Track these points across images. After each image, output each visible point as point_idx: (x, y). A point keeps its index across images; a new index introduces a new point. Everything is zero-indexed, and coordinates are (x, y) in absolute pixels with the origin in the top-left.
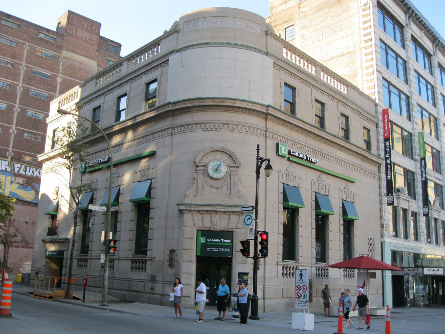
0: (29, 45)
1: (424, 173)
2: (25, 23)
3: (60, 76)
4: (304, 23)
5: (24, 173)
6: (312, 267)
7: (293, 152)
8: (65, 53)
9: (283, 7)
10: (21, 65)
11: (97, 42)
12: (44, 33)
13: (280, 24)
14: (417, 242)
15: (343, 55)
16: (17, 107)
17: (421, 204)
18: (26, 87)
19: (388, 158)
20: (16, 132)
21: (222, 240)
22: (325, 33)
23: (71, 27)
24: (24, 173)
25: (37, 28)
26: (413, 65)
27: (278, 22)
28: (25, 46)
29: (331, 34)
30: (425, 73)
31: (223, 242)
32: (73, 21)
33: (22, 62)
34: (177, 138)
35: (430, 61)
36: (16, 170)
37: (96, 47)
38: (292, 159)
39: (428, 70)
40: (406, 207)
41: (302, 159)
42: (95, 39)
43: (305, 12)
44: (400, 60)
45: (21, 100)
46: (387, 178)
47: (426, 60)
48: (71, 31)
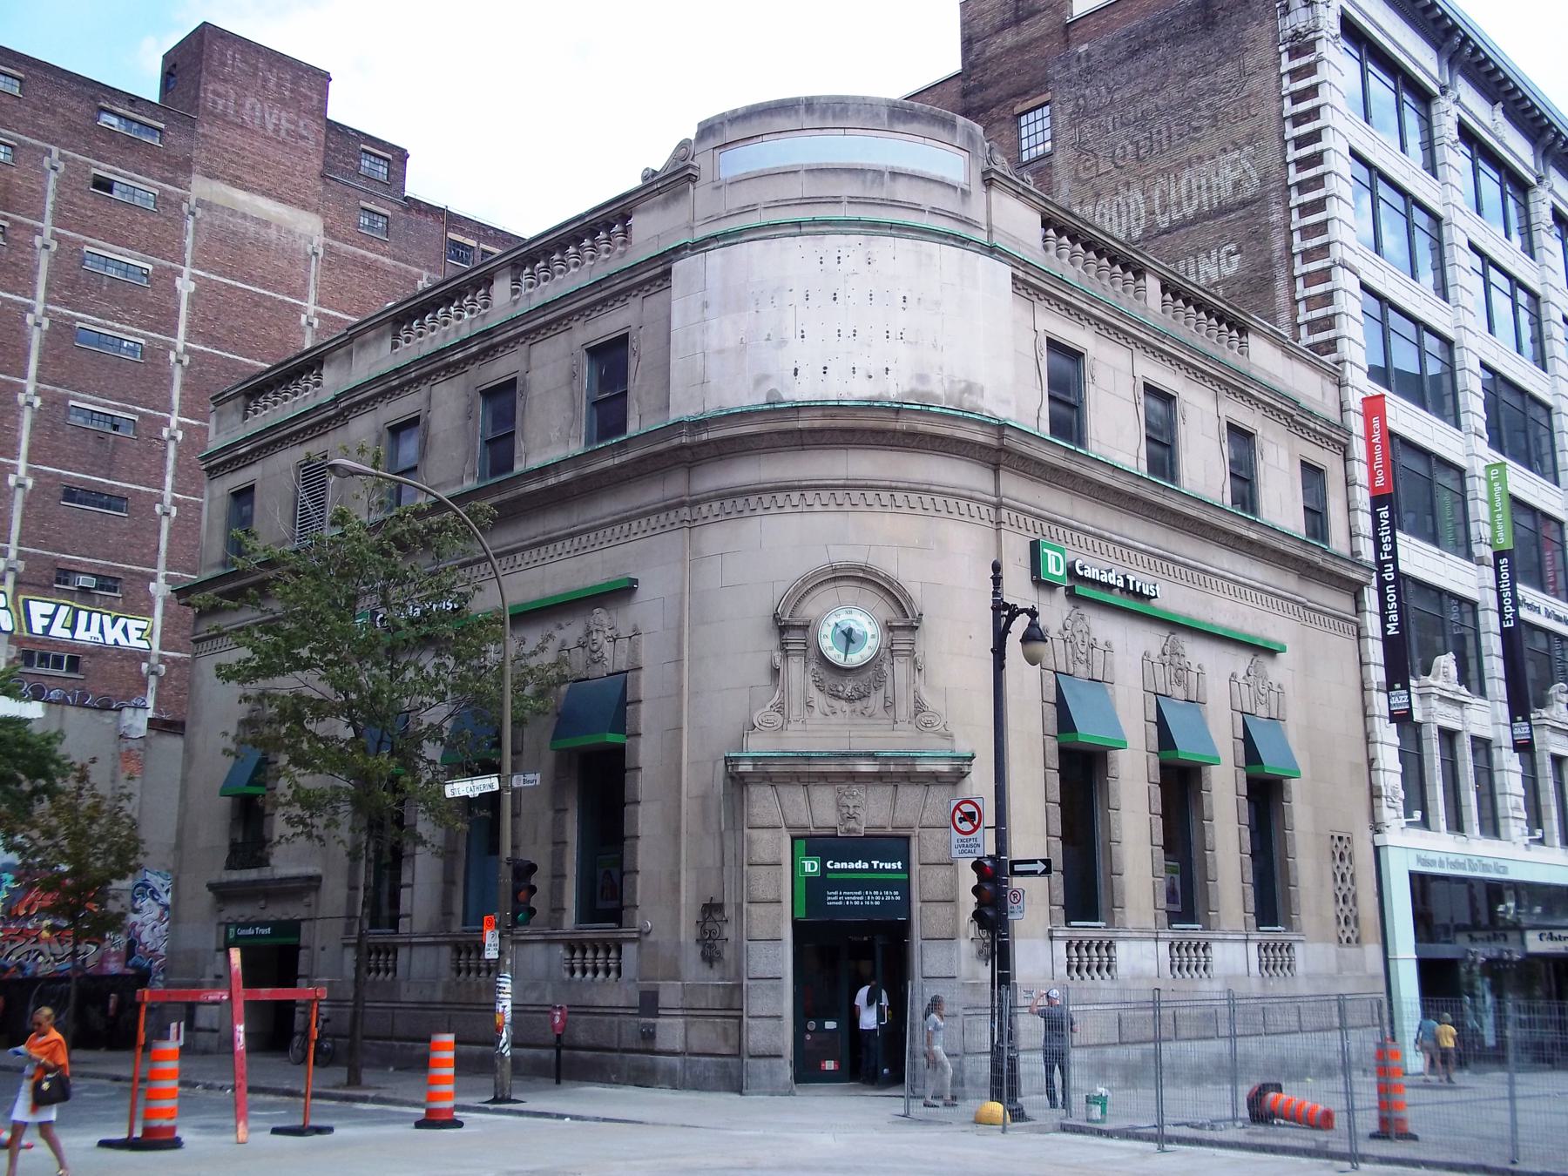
0: (62, 157)
1: (1508, 602)
2: (40, 74)
3: (187, 271)
4: (1083, 96)
5: (67, 634)
6: (1156, 940)
7: (1082, 569)
8: (201, 188)
9: (1009, 38)
10: (40, 232)
11: (318, 144)
12: (120, 110)
13: (999, 101)
14: (1496, 842)
15: (1222, 210)
16: (30, 389)
17: (1503, 710)
18: (62, 316)
19: (1387, 562)
20: (30, 483)
21: (875, 863)
22: (1159, 132)
23: (221, 89)
24: (67, 634)
25: (91, 92)
26: (1463, 227)
27: (992, 93)
28: (46, 159)
29: (1181, 136)
30: (1508, 253)
31: (878, 870)
32: (224, 64)
33: (42, 221)
34: (714, 537)
35: (1524, 209)
36: (38, 625)
37: (316, 163)
38: (1081, 590)
39: (1516, 241)
40: (1456, 726)
41: (1109, 587)
42: (313, 138)
43: (1088, 55)
44: (1420, 218)
45: (41, 362)
46: (1384, 630)
47: (1511, 202)
48: (221, 102)
